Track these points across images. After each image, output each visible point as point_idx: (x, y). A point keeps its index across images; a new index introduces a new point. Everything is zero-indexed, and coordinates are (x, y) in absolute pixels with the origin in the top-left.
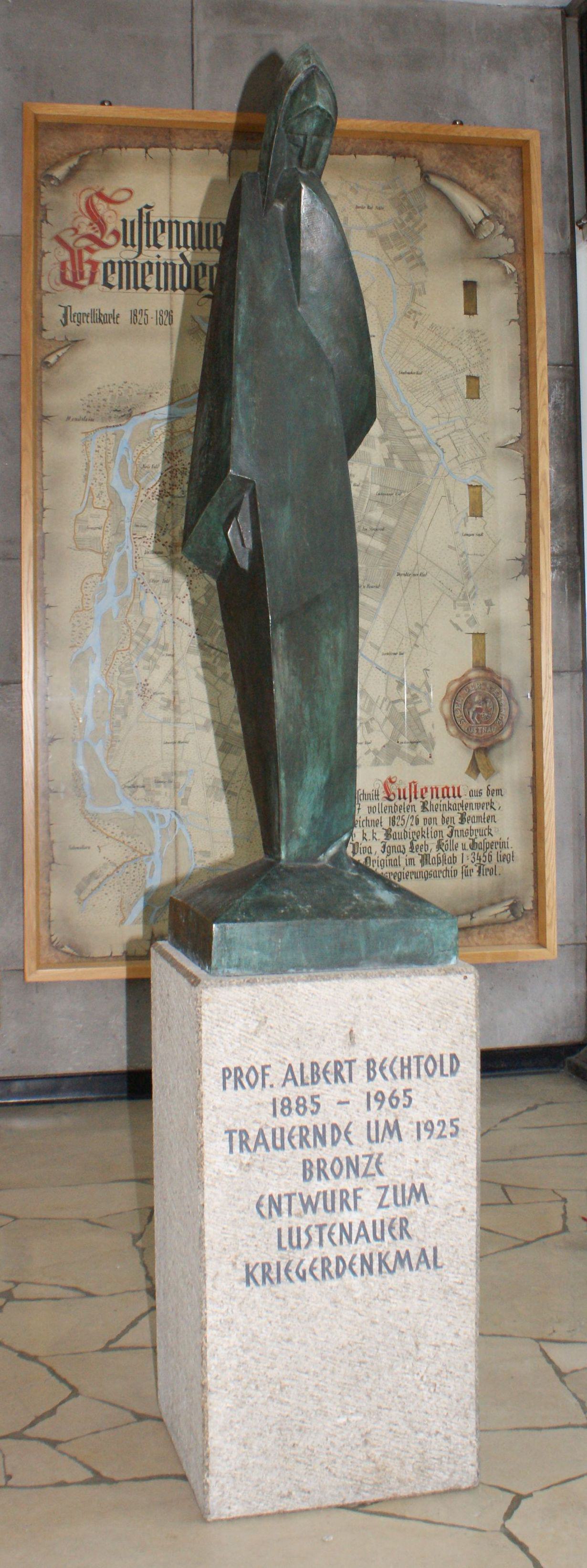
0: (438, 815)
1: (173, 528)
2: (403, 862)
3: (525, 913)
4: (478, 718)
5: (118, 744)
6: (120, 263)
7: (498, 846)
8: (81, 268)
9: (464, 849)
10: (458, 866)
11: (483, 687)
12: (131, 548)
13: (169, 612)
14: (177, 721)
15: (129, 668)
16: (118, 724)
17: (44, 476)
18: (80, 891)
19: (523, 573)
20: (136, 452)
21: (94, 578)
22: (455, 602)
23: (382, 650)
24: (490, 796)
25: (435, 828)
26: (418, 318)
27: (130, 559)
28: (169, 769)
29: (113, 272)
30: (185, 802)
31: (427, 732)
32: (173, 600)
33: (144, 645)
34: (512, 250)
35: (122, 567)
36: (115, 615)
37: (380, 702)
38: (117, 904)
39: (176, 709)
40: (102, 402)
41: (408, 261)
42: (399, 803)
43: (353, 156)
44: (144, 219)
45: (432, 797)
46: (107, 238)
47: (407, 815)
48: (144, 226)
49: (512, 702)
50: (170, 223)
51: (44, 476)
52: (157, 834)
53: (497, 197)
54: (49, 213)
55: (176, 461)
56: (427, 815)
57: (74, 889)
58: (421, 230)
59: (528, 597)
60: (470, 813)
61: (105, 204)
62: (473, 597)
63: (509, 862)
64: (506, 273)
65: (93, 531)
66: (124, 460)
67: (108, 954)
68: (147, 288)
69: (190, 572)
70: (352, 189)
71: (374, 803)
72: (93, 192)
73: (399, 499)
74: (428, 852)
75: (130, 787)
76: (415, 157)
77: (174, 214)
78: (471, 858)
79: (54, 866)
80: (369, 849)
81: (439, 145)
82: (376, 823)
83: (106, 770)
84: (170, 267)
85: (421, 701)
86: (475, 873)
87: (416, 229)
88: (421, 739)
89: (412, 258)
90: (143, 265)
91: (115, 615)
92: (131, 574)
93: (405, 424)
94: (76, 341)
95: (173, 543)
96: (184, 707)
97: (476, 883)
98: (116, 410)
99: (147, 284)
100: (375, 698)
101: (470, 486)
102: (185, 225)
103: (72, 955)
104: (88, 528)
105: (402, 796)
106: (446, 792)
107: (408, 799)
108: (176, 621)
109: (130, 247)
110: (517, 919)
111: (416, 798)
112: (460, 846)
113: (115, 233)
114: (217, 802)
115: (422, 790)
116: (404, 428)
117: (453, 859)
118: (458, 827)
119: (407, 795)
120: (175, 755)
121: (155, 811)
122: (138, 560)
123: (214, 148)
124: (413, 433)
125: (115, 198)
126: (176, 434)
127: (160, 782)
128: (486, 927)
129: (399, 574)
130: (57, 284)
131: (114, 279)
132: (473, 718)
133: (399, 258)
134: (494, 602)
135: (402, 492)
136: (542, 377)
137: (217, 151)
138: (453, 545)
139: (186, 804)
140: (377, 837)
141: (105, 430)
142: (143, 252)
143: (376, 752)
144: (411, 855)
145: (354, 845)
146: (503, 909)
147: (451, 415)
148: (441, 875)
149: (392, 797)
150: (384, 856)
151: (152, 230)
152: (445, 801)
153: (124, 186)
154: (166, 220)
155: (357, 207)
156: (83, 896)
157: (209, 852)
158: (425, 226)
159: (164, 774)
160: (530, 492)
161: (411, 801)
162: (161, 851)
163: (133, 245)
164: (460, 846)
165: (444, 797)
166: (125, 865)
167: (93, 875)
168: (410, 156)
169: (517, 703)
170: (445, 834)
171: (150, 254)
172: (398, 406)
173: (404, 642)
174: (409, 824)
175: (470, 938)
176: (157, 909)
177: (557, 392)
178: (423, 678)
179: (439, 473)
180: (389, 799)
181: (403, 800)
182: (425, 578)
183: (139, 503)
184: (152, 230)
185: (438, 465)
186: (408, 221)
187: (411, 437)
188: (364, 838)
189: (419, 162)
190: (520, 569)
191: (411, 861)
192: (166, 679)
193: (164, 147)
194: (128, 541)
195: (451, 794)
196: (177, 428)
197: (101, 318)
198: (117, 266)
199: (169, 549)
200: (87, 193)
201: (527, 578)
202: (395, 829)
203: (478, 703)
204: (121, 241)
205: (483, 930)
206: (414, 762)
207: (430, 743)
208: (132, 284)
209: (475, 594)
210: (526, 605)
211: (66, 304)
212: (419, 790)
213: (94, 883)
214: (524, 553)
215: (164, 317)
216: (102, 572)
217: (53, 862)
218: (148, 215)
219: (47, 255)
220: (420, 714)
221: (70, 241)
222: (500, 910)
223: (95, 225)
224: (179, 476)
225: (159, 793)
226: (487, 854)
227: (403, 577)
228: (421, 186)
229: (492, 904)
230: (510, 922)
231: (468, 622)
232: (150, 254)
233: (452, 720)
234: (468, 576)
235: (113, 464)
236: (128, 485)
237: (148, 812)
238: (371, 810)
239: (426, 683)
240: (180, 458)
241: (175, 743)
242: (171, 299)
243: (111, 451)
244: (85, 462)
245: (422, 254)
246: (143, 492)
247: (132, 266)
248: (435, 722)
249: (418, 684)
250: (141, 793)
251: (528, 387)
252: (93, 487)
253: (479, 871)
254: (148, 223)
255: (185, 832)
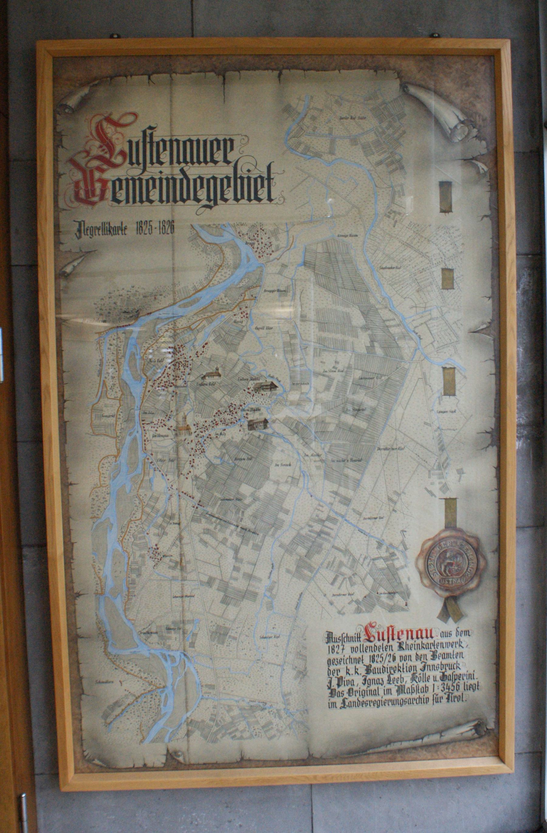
0: (413, 653)
1: (177, 414)
2: (381, 692)
3: (488, 732)
4: (449, 572)
5: (134, 598)
6: (127, 180)
7: (465, 678)
8: (93, 185)
9: (435, 680)
10: (429, 694)
11: (454, 545)
12: (140, 432)
13: (175, 487)
14: (184, 579)
15: (141, 535)
16: (133, 582)
17: (64, 372)
18: (106, 716)
19: (492, 444)
20: (143, 348)
21: (110, 458)
22: (429, 471)
23: (364, 515)
24: (459, 637)
25: (410, 663)
26: (398, 217)
27: (139, 442)
28: (178, 618)
29: (121, 188)
30: (192, 645)
31: (404, 584)
32: (179, 476)
33: (154, 515)
34: (484, 151)
35: (133, 449)
36: (128, 491)
37: (361, 560)
38: (138, 726)
39: (182, 569)
40: (113, 305)
41: (388, 165)
42: (378, 644)
43: (337, 71)
44: (148, 139)
45: (408, 638)
46: (115, 158)
47: (385, 653)
48: (148, 146)
49: (480, 557)
50: (171, 141)
51: (64, 372)
52: (169, 671)
53: (470, 103)
54: (64, 139)
55: (179, 355)
56: (403, 653)
57: (101, 714)
58: (401, 136)
59: (496, 465)
60: (440, 651)
61: (113, 128)
62: (446, 467)
63: (474, 690)
64: (478, 173)
65: (107, 419)
66: (133, 355)
67: (132, 766)
68: (151, 202)
69: (193, 452)
70: (337, 102)
71: (356, 644)
72: (102, 117)
73: (379, 382)
74: (404, 683)
75: (144, 633)
76: (394, 69)
77: (175, 133)
78: (441, 688)
79: (83, 696)
80: (352, 682)
81: (418, 57)
82: (358, 660)
83: (125, 620)
84: (171, 181)
85: (398, 558)
86: (444, 700)
87: (396, 136)
88: (397, 590)
89: (392, 163)
90: (147, 181)
91: (128, 491)
92: (141, 455)
93: (385, 314)
94: (90, 252)
95: (177, 427)
96: (189, 567)
97: (444, 708)
98: (125, 312)
99: (151, 198)
100: (357, 556)
101: (444, 368)
102: (185, 143)
103: (101, 767)
104: (103, 416)
105: (381, 638)
106: (419, 634)
107: (386, 641)
108: (181, 494)
109: (135, 165)
110: (481, 737)
111: (393, 639)
112: (432, 678)
113: (122, 153)
114: (219, 645)
115: (398, 633)
116: (384, 319)
117: (426, 689)
118: (430, 662)
119: (386, 637)
120: (183, 608)
121: (167, 653)
122: (146, 443)
123: (209, 72)
124: (392, 323)
125: (122, 122)
126: (178, 331)
127: (170, 629)
128: (453, 744)
129: (379, 449)
130: (72, 202)
131: (121, 195)
132: (445, 571)
133: (380, 163)
134: (465, 470)
135: (382, 375)
136: (511, 269)
137: (212, 74)
138: (428, 421)
139: (194, 647)
140: (359, 672)
141: (115, 330)
142: (148, 169)
143: (357, 602)
144: (388, 686)
145: (339, 679)
146: (469, 729)
147: (428, 305)
148: (415, 702)
149: (372, 639)
150: (365, 687)
151: (155, 149)
152: (419, 641)
153: (128, 111)
154: (167, 139)
155: (341, 118)
156: (109, 720)
157: (214, 686)
158: (404, 132)
159: (174, 623)
160: (500, 372)
161: (388, 642)
162: (173, 685)
163: (138, 163)
164: (432, 678)
165: (417, 638)
166: (143, 696)
167: (117, 704)
168: (390, 69)
169: (485, 558)
170: (418, 669)
171: (153, 171)
172: (380, 299)
173: (383, 508)
174: (387, 660)
175: (439, 753)
176: (171, 730)
177: (525, 279)
178: (401, 538)
179: (416, 358)
180: (369, 640)
181: (382, 641)
182: (402, 451)
183: (147, 393)
184: (155, 149)
185: (416, 350)
186: (388, 129)
187: (391, 326)
188: (347, 673)
189: (398, 74)
190: (489, 442)
191: (389, 691)
192: (174, 544)
193: (165, 73)
194: (138, 427)
195: (424, 635)
196: (179, 326)
197: (109, 230)
198: (124, 183)
199: (174, 433)
200: (98, 119)
201: (495, 448)
202: (374, 665)
203: (450, 558)
204: (128, 161)
205: (451, 746)
206: (392, 609)
207: (406, 594)
208: (138, 199)
209: (448, 464)
210: (493, 472)
211: (79, 220)
212: (396, 633)
213: (118, 711)
214: (493, 427)
215: (167, 226)
216: (116, 454)
217: (83, 693)
218: (151, 135)
219: (62, 177)
220: (397, 569)
221: (83, 163)
222: (466, 730)
223: (104, 147)
224: (182, 368)
225: (170, 638)
226: (455, 685)
227: (383, 451)
228: (400, 96)
229: (459, 725)
230: (474, 739)
231: (441, 489)
232: (153, 171)
233: (426, 573)
234: (442, 449)
235: (123, 359)
236: (137, 378)
237: (161, 653)
238: (353, 649)
239: (403, 543)
240: (182, 352)
241: (182, 597)
242: (173, 211)
243: (122, 349)
244: (99, 358)
245: (402, 158)
246: (150, 383)
247: (137, 182)
248: (410, 574)
249: (396, 543)
250: (154, 638)
251: (499, 277)
252: (106, 380)
253: (448, 699)
254: (151, 142)
255: (192, 669)
